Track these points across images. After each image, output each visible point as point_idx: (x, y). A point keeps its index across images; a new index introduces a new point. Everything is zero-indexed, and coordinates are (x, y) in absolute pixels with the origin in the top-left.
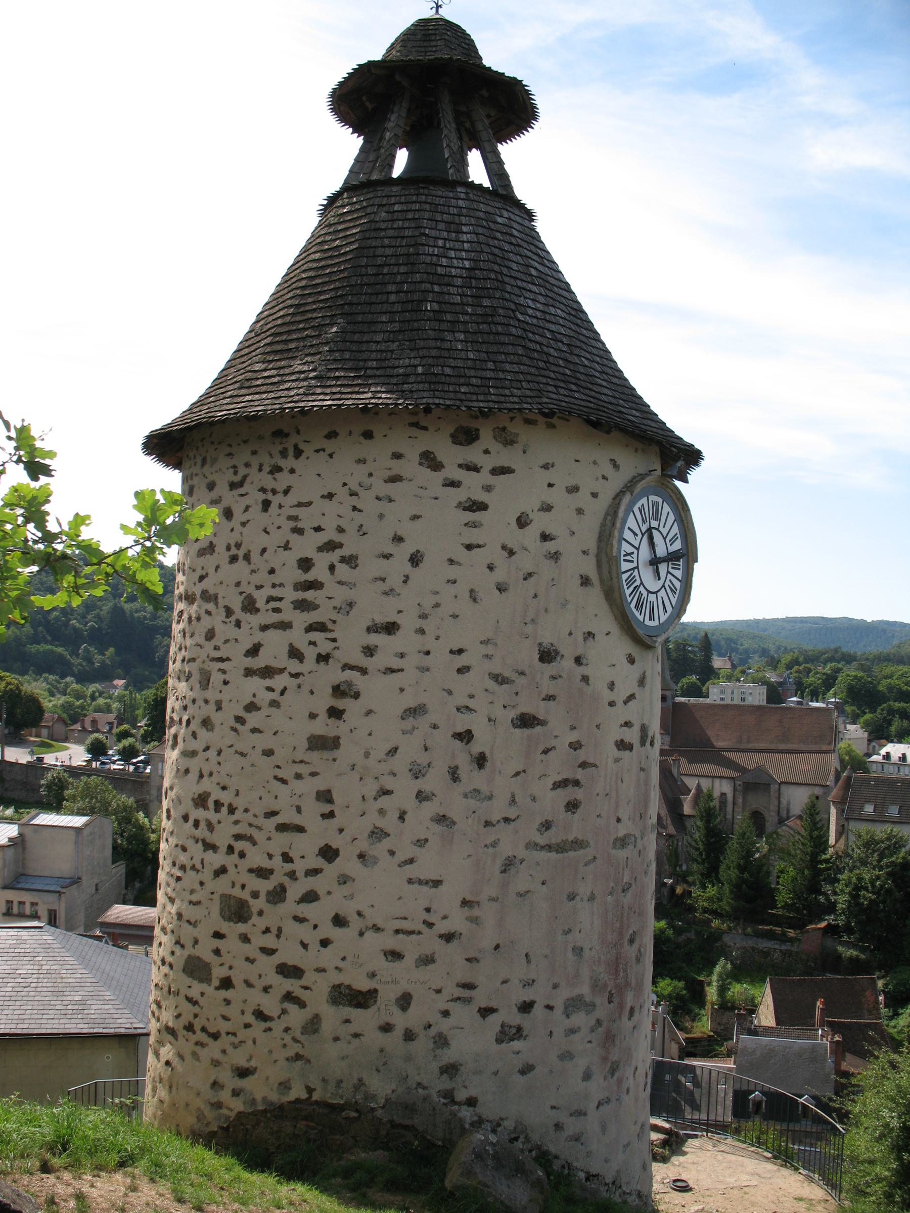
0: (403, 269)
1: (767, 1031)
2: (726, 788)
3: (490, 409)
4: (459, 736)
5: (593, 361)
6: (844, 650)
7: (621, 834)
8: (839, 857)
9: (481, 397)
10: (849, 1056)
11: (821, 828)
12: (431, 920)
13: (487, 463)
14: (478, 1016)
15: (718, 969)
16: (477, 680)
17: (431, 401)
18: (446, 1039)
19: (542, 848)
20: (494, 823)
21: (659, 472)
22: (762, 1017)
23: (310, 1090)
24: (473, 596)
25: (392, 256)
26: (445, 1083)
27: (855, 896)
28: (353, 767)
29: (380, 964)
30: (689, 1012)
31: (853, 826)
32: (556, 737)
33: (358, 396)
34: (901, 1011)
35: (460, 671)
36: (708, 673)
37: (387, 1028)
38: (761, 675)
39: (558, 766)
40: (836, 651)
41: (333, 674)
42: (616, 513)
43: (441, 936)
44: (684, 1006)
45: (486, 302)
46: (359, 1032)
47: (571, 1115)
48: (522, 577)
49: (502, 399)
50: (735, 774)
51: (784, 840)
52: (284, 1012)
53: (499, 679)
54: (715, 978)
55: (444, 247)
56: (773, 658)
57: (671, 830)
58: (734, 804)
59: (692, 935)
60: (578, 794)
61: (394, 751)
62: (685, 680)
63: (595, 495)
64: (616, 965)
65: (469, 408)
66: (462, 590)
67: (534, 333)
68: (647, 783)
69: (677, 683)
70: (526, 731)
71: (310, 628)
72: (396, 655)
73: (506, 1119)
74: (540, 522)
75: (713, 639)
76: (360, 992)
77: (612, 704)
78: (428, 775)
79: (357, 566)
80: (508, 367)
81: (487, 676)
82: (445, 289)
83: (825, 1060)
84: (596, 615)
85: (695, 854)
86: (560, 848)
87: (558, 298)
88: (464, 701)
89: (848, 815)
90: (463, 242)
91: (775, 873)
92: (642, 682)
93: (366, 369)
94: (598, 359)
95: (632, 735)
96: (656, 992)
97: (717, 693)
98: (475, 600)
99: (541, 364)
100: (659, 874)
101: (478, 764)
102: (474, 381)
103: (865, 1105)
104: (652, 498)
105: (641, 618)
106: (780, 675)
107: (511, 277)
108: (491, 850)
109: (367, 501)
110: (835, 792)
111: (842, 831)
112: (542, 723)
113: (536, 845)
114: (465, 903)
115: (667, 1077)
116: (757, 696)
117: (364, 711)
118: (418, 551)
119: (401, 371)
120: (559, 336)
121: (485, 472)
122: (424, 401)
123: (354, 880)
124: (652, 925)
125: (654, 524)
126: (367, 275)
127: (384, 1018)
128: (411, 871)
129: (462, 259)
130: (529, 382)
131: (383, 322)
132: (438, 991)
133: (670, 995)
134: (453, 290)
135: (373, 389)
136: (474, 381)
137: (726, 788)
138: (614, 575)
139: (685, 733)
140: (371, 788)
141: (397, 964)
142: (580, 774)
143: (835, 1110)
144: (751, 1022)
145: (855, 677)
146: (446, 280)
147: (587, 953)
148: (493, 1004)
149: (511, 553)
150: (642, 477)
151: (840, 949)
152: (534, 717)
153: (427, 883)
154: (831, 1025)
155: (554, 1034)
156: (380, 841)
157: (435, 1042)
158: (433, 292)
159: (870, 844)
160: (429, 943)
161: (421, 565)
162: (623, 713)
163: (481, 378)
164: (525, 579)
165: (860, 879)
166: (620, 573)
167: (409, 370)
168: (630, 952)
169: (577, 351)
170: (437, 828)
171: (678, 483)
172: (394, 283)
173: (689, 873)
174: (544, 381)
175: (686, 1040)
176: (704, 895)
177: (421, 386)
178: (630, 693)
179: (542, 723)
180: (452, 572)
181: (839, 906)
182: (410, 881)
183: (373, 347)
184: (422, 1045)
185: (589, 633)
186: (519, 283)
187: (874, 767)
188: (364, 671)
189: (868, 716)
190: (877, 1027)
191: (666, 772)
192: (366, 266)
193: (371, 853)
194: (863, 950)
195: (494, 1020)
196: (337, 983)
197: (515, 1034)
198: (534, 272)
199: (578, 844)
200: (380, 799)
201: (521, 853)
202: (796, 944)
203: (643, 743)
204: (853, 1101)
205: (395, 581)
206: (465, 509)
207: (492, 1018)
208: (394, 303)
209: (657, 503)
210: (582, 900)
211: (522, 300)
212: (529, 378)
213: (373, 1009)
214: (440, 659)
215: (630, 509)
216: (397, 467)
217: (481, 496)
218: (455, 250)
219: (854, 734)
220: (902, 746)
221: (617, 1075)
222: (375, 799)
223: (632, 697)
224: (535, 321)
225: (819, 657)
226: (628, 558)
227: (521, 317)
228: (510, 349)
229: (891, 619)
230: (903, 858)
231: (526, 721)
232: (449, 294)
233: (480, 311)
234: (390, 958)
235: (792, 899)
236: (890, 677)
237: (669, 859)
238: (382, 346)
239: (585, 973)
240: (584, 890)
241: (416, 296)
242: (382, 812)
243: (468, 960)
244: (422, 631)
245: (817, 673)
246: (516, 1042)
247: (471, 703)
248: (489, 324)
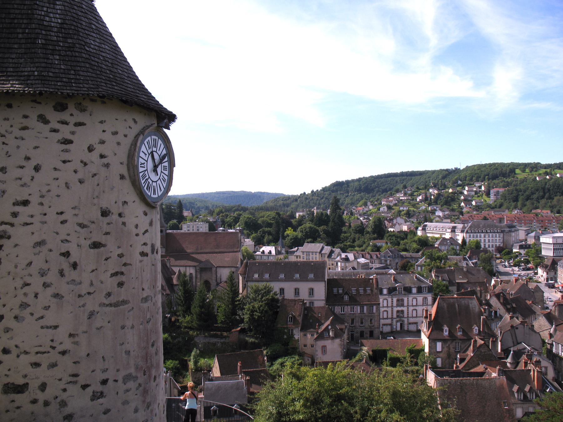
0: (25, 21)
1: (217, 379)
2: (192, 271)
3: (73, 94)
4: (63, 254)
5: (124, 71)
6: (243, 205)
7: (144, 296)
8: (244, 298)
9: (68, 88)
10: (253, 385)
11: (236, 286)
12: (54, 345)
13: (72, 120)
14: (81, 390)
15: (193, 353)
16: (71, 226)
17: (42, 89)
18: (65, 403)
19: (107, 305)
21: (156, 125)
22: (214, 373)
24: (67, 186)
25: (19, 14)
27: (252, 315)
28: (9, 273)
29: (30, 370)
30: (181, 374)
31: (249, 284)
32: (111, 252)
33: (3, 86)
34: (274, 363)
35: (62, 223)
36: (182, 219)
37: (34, 401)
38: (205, 218)
39: (113, 266)
40: (239, 206)
42: (136, 144)
43: (60, 353)
44: (178, 372)
45: (70, 41)
46: (19, 405)
48: (91, 176)
49: (79, 89)
50: (196, 264)
51: (219, 293)
54: (192, 357)
55: (47, 11)
56: (211, 210)
57: (168, 292)
58: (196, 278)
59: (180, 339)
61: (30, 264)
62: (171, 222)
63: (126, 136)
64: (146, 357)
65: (62, 93)
67: (94, 57)
68: (156, 271)
69: (167, 224)
70: (96, 250)
72: (29, 216)
74: (99, 149)
75: (183, 202)
76: (19, 386)
77: (137, 235)
79: (6, 172)
80: (81, 73)
81: (76, 225)
82: (48, 33)
83: (243, 388)
85: (179, 302)
86: (116, 305)
87: (106, 40)
88: (65, 237)
89: (247, 279)
90: (57, 9)
91: (216, 308)
92: (151, 224)
93: (7, 72)
94: (126, 71)
95: (148, 249)
96: (166, 367)
97: (186, 228)
98: (68, 188)
99: (98, 72)
100: (164, 312)
102: (64, 80)
103: (261, 406)
104: (153, 137)
105: (149, 194)
106: (214, 218)
107: (82, 28)
108: (82, 308)
110: (241, 270)
111: (244, 287)
112: (104, 246)
113: (104, 304)
114: (71, 335)
115: (174, 405)
116: (204, 228)
117: (13, 245)
118: (38, 164)
119: (26, 74)
120: (107, 59)
121: (71, 125)
122: (39, 89)
123: (12, 330)
124: (162, 336)
125: (154, 149)
126: (5, 23)
127: (33, 396)
128: (42, 322)
129: (57, 18)
130: (92, 81)
131: (15, 48)
132: (60, 380)
133: (172, 368)
134: (53, 34)
135: (11, 82)
136: (64, 80)
137: (192, 271)
138: (136, 174)
139: (172, 247)
140: (19, 283)
141: (38, 369)
142: (123, 269)
143: (248, 409)
144: (210, 375)
145: (248, 218)
146: (48, 28)
147: (132, 353)
148: (88, 383)
149: (85, 164)
150: (148, 127)
151: (247, 339)
152: (100, 243)
153: (51, 327)
154: (244, 372)
155: (119, 393)
156: (25, 309)
157: (60, 405)
158: (42, 34)
159: (257, 291)
160: (54, 356)
162: (142, 239)
163: (68, 79)
164: (93, 177)
165: (254, 307)
166: (139, 173)
167: (30, 73)
168: (153, 350)
169: (116, 67)
170: (55, 300)
171: (165, 130)
172: (21, 28)
173: (177, 311)
174: (100, 80)
175: (181, 387)
176: (185, 320)
177: (37, 82)
178: (149, 231)
179: (104, 246)
180: (56, 174)
181: (245, 320)
182: (42, 327)
183: (11, 61)
184: (53, 408)
185: (125, 202)
186: (87, 32)
187: (257, 257)
188: (12, 225)
189: (254, 235)
190: (264, 371)
191: (164, 265)
192: (5, 18)
193: (21, 315)
194: (256, 338)
195: (89, 390)
196: (6, 383)
198: (94, 27)
199: (124, 302)
200: (24, 288)
201: (97, 309)
202: (227, 339)
203: (153, 253)
204: (256, 404)
205: (27, 179)
206: (61, 143)
208: (21, 39)
209: (156, 140)
211: (88, 41)
212: (92, 79)
213: (27, 393)
214: (52, 217)
215: (142, 142)
216: (25, 122)
217: (70, 137)
218: (53, 13)
219: (248, 243)
220: (269, 247)
221: (150, 408)
222: (22, 288)
223: (146, 231)
224: (95, 51)
225: (231, 209)
226: (142, 165)
227: (87, 49)
228: (83, 64)
229: (263, 191)
230: (272, 296)
231: (96, 245)
232: (51, 35)
233: (66, 45)
234: (34, 366)
235: (224, 319)
236: (263, 217)
237: (168, 305)
238: (16, 61)
239: (132, 362)
240: (129, 324)
241: (33, 36)
242: (25, 294)
244: (42, 204)
245: (230, 217)
247: (68, 238)
248: (71, 51)
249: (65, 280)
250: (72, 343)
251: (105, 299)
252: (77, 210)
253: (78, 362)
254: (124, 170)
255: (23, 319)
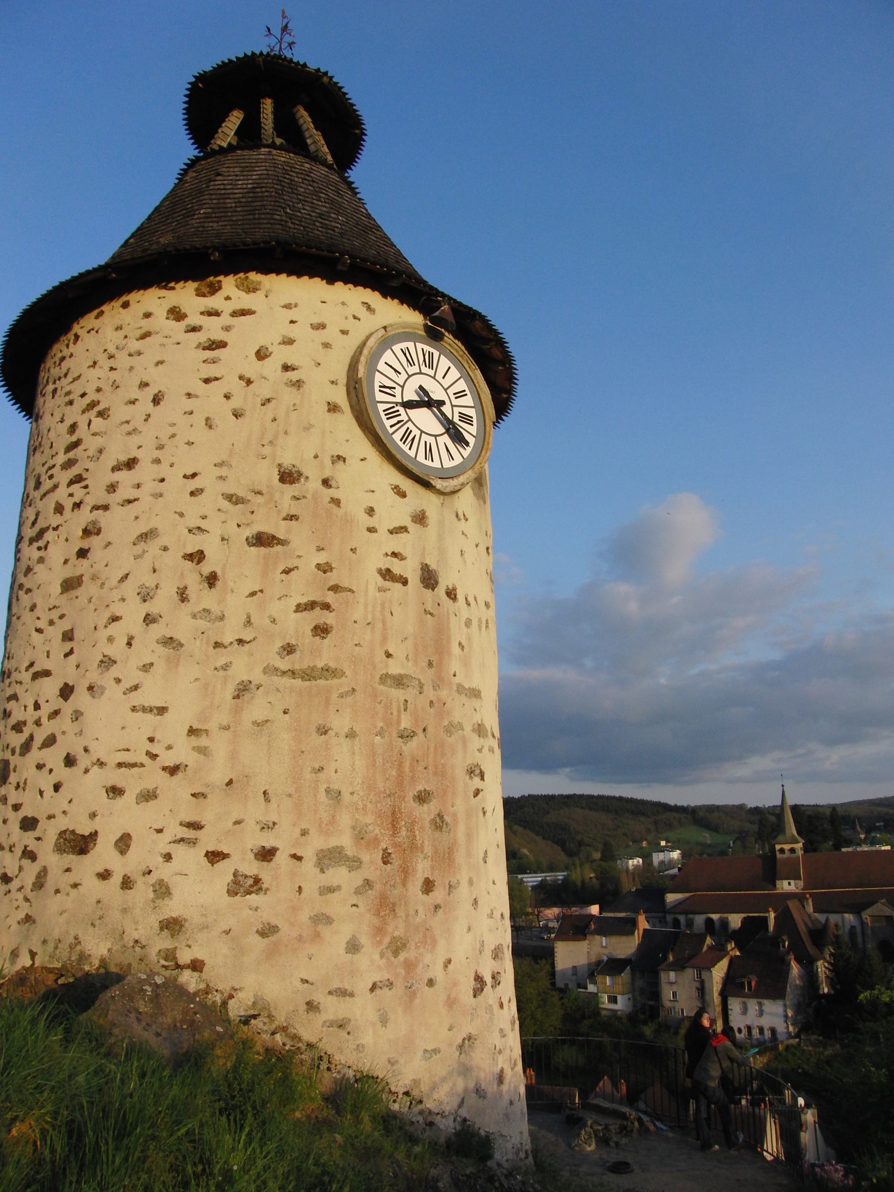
4: (190, 557)
13: (227, 308)
16: (211, 500)
18: (167, 888)
19: (284, 673)
20: (226, 644)
23: (33, 955)
24: (209, 423)
26: (164, 942)
32: (299, 557)
35: (192, 494)
37: (104, 875)
39: (302, 588)
41: (85, 516)
47: (330, 993)
48: (259, 403)
52: (21, 869)
53: (233, 499)
60: (329, 618)
63: (344, 332)
66: (199, 420)
70: (263, 550)
71: (71, 483)
73: (241, 989)
78: (156, 597)
79: (108, 416)
84: (347, 441)
86: (308, 675)
98: (210, 427)
101: (209, 583)
108: (221, 673)
109: (122, 361)
112: (282, 542)
113: (276, 669)
114: (192, 732)
128: (137, 699)
132: (160, 831)
142: (330, 598)
147: (346, 797)
149: (249, 382)
152: (274, 537)
153: (151, 711)
155: (304, 890)
156: (108, 669)
160: (153, 777)
161: (162, 403)
164: (263, 405)
170: (161, 650)
179: (282, 542)
180: (189, 404)
182: (134, 709)
185: (339, 457)
193: (99, 683)
195: (226, 870)
197: (251, 886)
199: (329, 672)
201: (257, 676)
207: (222, 865)
209: (431, 355)
210: (337, 735)
222: (106, 627)
231: (261, 540)
234: (111, 795)
239: (345, 820)
240: (340, 723)
243: (193, 795)
246: (253, 895)
247: (203, 524)
249: (187, 608)
250: (194, 748)
251: (277, 657)
252: (225, 469)
253: (204, 795)
254: (340, 396)
255: (103, 689)
